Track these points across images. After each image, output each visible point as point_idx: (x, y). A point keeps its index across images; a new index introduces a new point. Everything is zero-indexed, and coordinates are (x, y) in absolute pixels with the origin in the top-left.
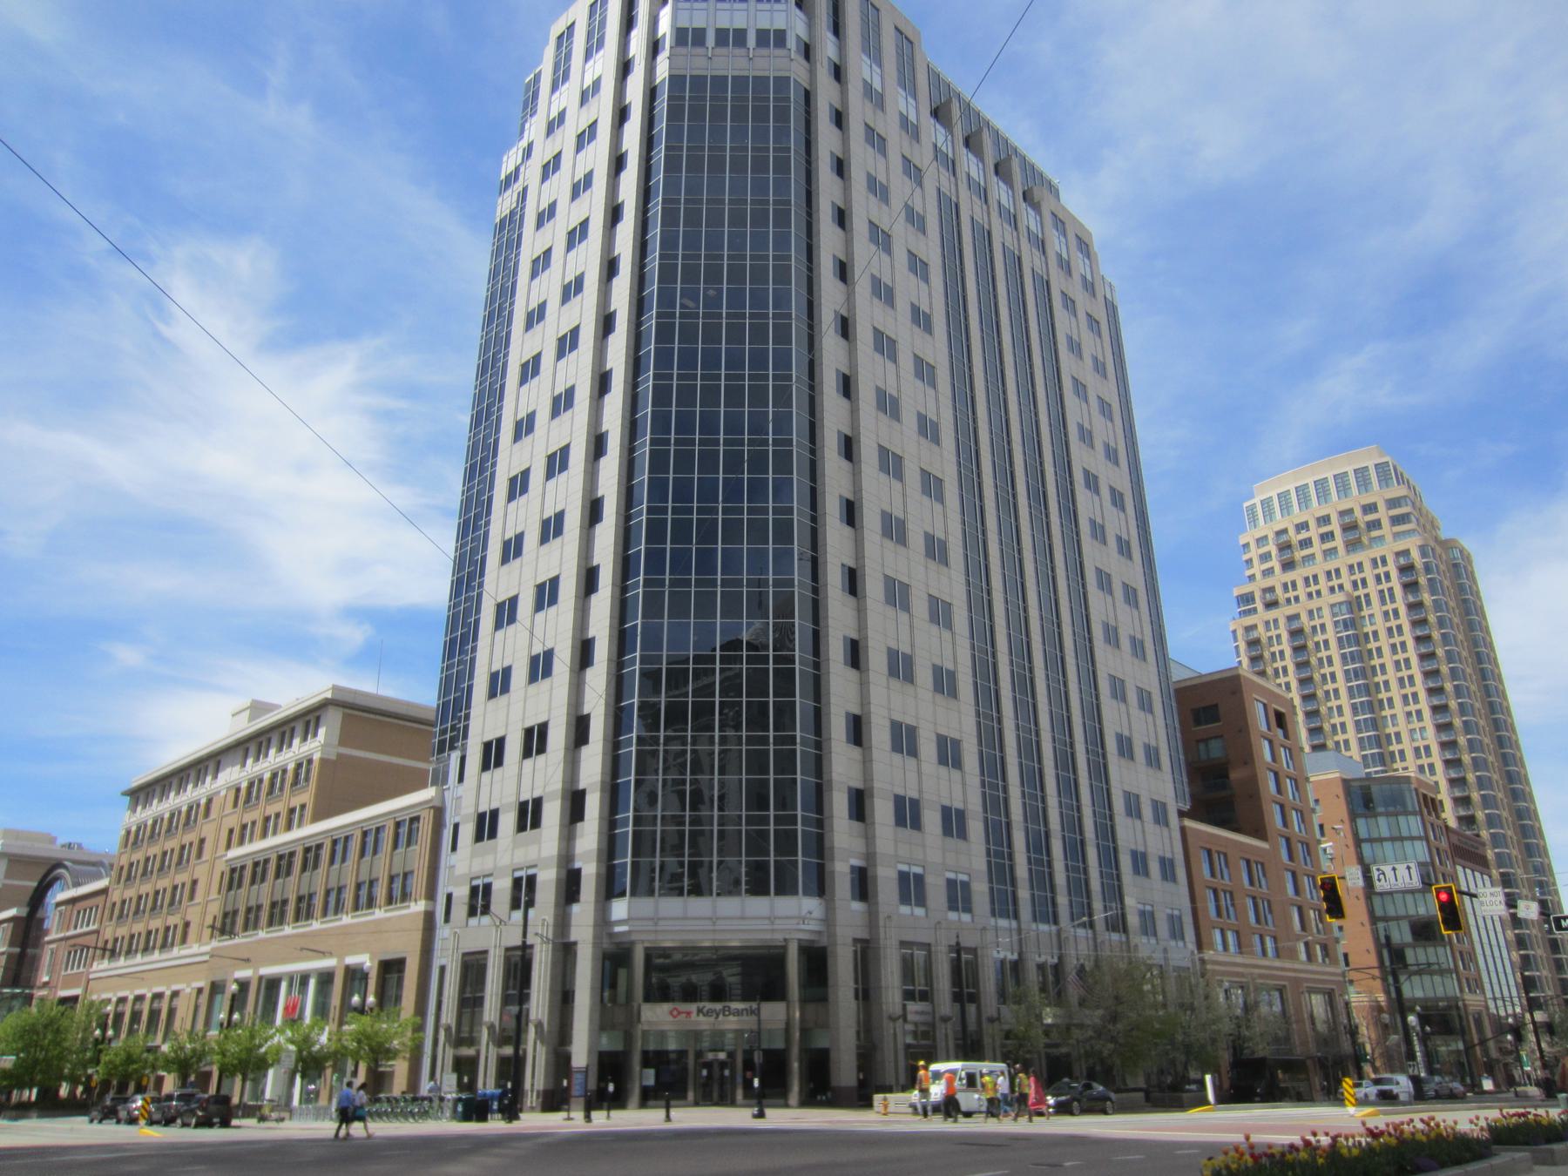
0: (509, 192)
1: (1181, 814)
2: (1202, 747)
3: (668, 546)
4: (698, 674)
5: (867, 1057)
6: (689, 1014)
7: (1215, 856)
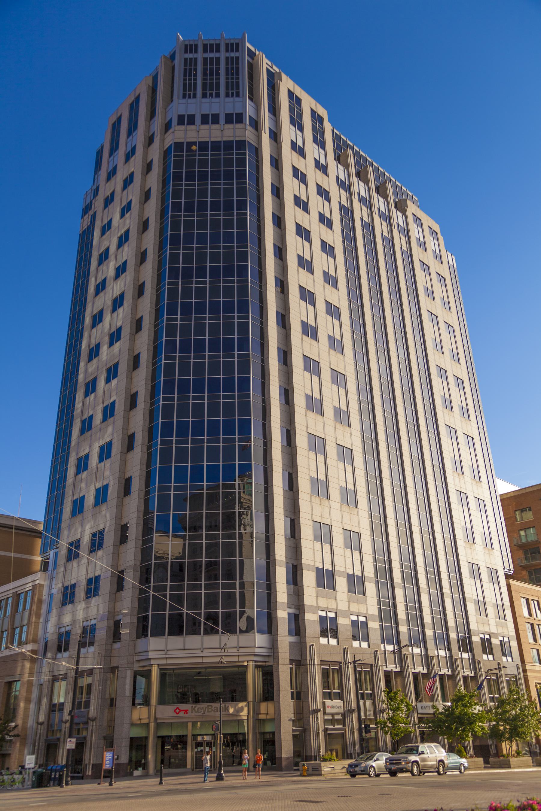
0: (87, 216)
1: (507, 576)
2: (522, 533)
3: (237, 418)
4: (225, 495)
5: (301, 738)
6: (186, 711)
7: (531, 603)
